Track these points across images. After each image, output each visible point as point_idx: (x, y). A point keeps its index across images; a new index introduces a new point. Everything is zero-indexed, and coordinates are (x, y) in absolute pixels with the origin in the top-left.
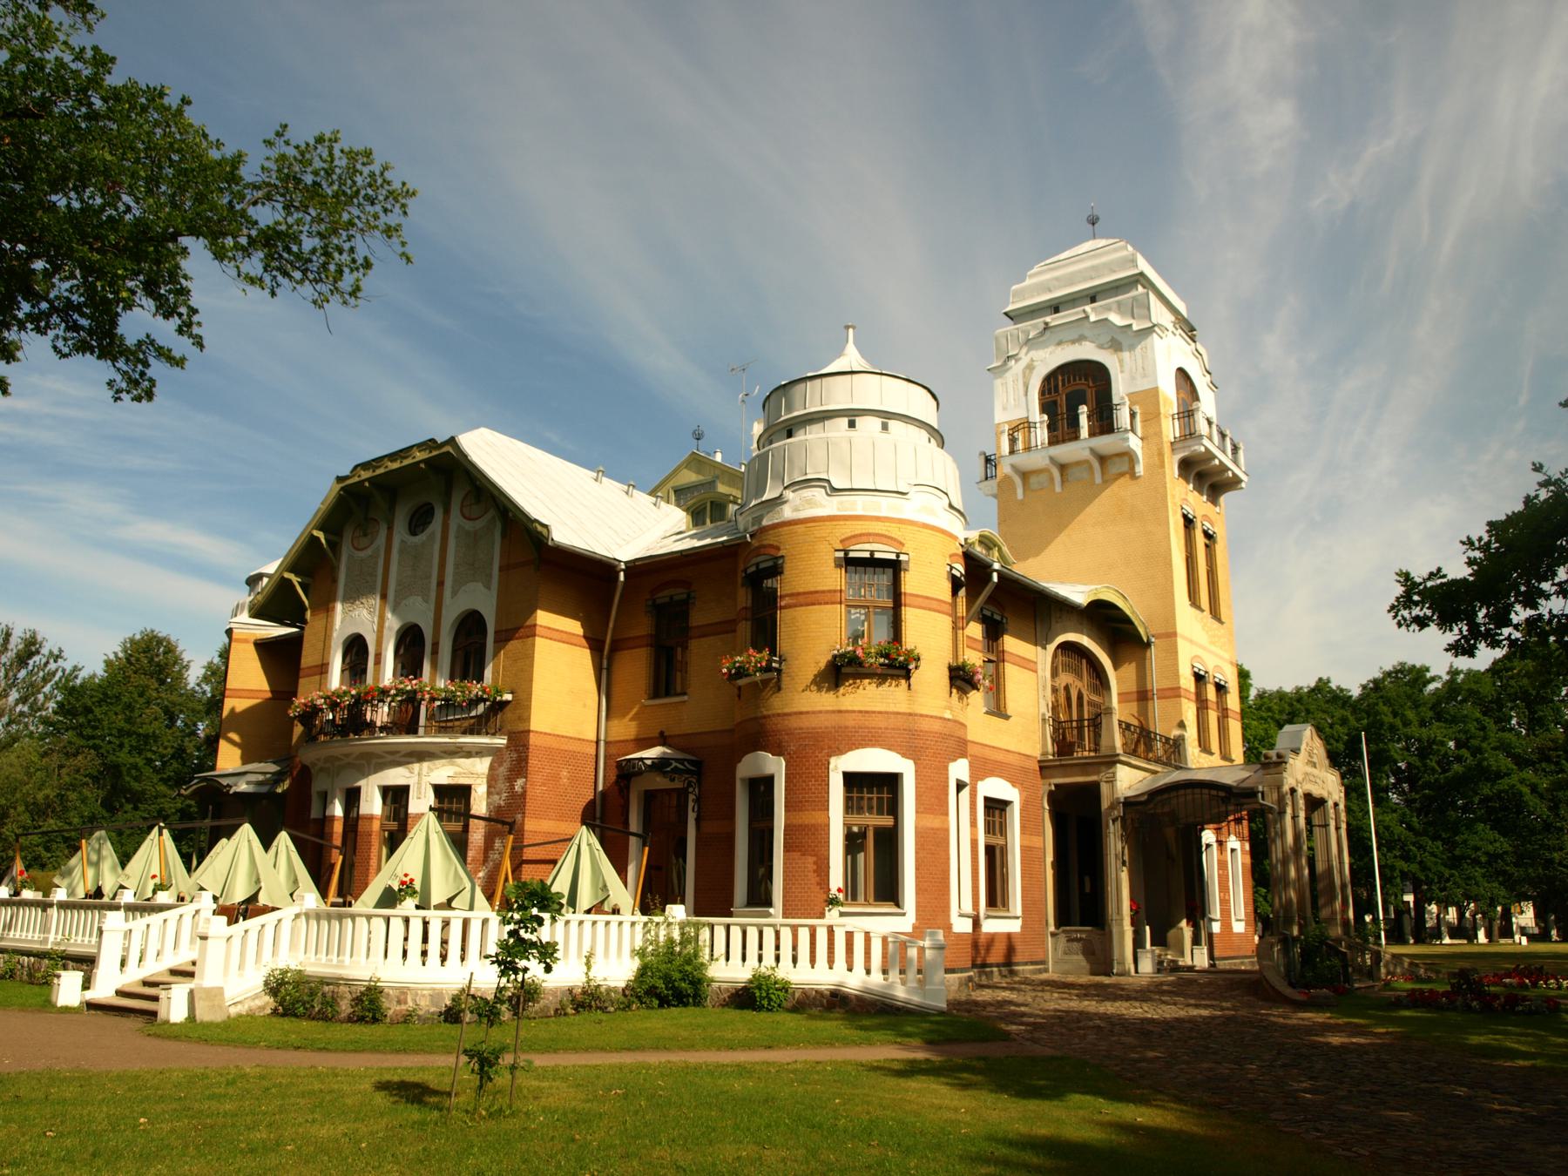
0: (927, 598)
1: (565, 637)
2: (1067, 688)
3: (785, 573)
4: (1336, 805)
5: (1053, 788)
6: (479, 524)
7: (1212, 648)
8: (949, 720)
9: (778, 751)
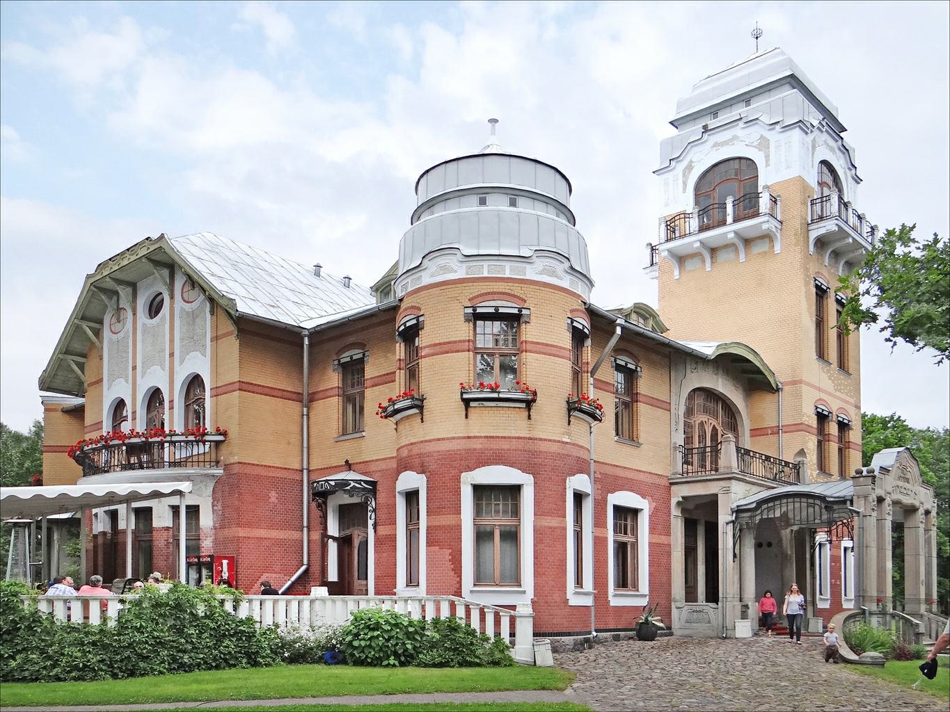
0: (547, 345)
2: (702, 424)
4: (927, 513)
5: (681, 499)
6: (195, 305)
7: (838, 394)
8: (567, 443)
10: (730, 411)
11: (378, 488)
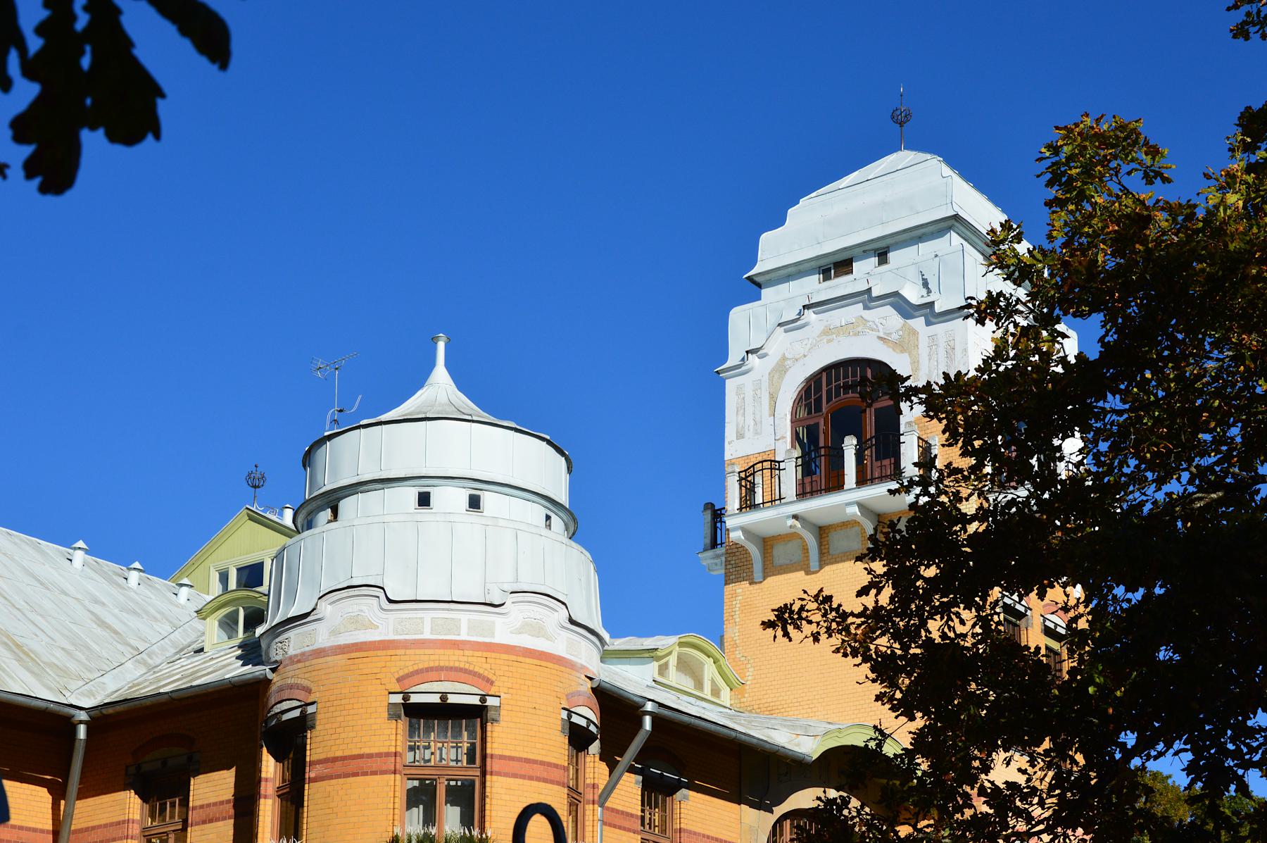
0: (528, 761)
1: (539, 771)
3: (318, 728)
10: (1015, 625)
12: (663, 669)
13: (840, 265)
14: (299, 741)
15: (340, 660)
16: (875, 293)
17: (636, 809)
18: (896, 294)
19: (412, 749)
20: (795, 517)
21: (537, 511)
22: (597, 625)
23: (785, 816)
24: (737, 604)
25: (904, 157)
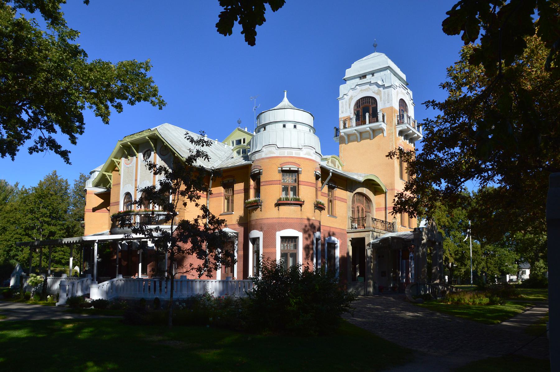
0: (307, 182)
1: (310, 184)
2: (358, 207)
9: (261, 230)
10: (368, 199)
11: (239, 235)
12: (328, 162)
13: (364, 76)
14: (172, 166)
15: (267, 160)
16: (372, 82)
17: (327, 192)
18: (376, 83)
19: (283, 179)
20: (355, 130)
21: (307, 129)
22: (320, 153)
23: (355, 194)
24: (342, 149)
25: (376, 54)
